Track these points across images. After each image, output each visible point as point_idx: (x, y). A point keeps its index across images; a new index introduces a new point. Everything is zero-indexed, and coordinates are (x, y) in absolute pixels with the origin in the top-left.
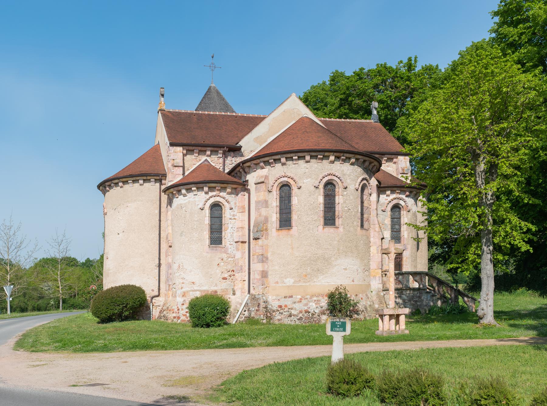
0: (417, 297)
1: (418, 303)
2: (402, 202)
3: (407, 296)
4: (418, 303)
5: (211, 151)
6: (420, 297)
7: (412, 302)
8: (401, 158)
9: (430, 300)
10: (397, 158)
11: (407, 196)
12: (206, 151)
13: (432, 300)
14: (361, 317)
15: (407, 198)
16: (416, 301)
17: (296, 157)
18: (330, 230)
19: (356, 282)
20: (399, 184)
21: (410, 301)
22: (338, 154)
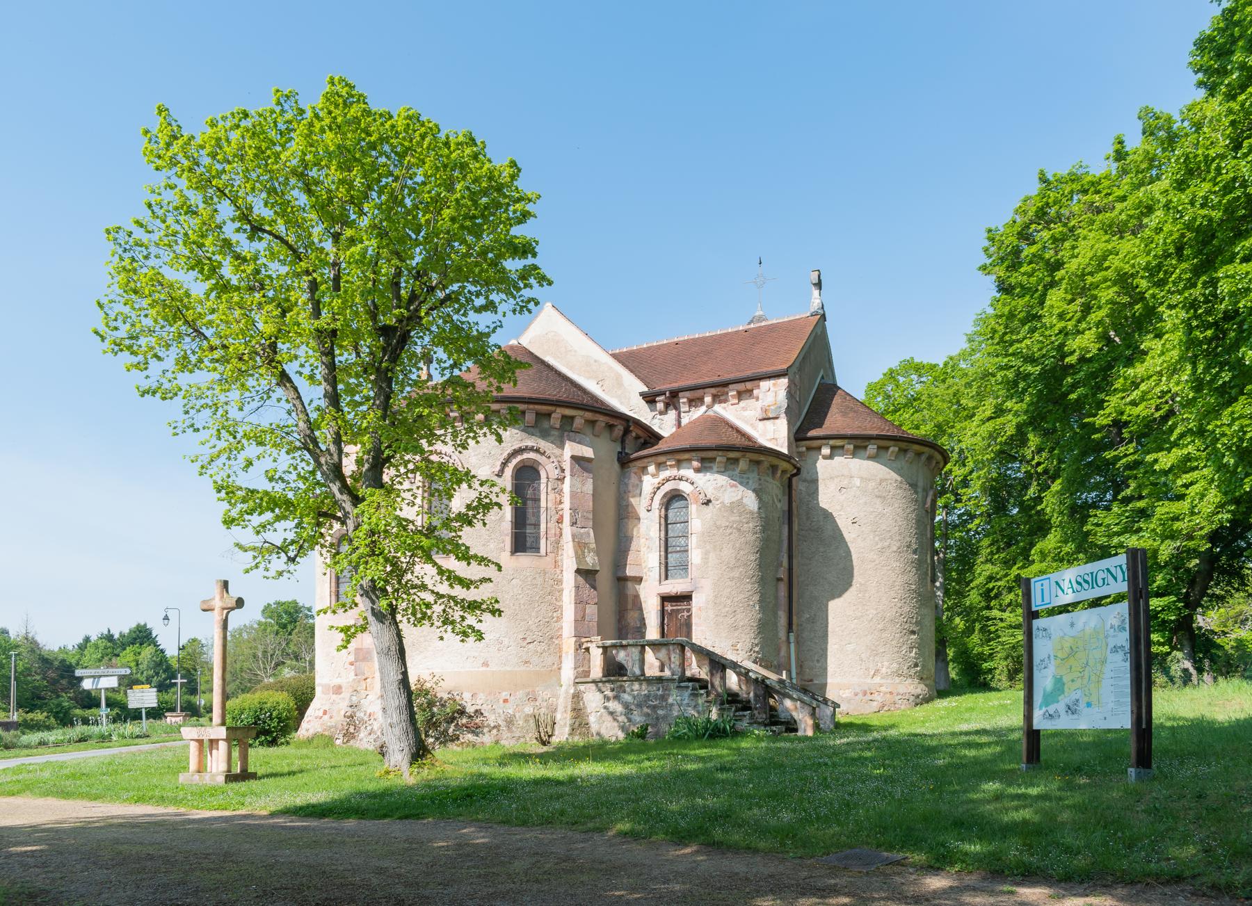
0: (656, 697)
1: (660, 712)
2: (685, 487)
3: (634, 697)
4: (660, 712)
5: (832, 448)
6: (663, 698)
7: (645, 710)
8: (764, 384)
9: (688, 705)
10: (758, 387)
11: (698, 470)
12: (819, 448)
13: (693, 703)
14: (487, 739)
15: (700, 475)
16: (654, 708)
17: (851, 447)
18: (524, 560)
19: (493, 667)
20: (577, 398)
21: (639, 706)
22: (904, 445)
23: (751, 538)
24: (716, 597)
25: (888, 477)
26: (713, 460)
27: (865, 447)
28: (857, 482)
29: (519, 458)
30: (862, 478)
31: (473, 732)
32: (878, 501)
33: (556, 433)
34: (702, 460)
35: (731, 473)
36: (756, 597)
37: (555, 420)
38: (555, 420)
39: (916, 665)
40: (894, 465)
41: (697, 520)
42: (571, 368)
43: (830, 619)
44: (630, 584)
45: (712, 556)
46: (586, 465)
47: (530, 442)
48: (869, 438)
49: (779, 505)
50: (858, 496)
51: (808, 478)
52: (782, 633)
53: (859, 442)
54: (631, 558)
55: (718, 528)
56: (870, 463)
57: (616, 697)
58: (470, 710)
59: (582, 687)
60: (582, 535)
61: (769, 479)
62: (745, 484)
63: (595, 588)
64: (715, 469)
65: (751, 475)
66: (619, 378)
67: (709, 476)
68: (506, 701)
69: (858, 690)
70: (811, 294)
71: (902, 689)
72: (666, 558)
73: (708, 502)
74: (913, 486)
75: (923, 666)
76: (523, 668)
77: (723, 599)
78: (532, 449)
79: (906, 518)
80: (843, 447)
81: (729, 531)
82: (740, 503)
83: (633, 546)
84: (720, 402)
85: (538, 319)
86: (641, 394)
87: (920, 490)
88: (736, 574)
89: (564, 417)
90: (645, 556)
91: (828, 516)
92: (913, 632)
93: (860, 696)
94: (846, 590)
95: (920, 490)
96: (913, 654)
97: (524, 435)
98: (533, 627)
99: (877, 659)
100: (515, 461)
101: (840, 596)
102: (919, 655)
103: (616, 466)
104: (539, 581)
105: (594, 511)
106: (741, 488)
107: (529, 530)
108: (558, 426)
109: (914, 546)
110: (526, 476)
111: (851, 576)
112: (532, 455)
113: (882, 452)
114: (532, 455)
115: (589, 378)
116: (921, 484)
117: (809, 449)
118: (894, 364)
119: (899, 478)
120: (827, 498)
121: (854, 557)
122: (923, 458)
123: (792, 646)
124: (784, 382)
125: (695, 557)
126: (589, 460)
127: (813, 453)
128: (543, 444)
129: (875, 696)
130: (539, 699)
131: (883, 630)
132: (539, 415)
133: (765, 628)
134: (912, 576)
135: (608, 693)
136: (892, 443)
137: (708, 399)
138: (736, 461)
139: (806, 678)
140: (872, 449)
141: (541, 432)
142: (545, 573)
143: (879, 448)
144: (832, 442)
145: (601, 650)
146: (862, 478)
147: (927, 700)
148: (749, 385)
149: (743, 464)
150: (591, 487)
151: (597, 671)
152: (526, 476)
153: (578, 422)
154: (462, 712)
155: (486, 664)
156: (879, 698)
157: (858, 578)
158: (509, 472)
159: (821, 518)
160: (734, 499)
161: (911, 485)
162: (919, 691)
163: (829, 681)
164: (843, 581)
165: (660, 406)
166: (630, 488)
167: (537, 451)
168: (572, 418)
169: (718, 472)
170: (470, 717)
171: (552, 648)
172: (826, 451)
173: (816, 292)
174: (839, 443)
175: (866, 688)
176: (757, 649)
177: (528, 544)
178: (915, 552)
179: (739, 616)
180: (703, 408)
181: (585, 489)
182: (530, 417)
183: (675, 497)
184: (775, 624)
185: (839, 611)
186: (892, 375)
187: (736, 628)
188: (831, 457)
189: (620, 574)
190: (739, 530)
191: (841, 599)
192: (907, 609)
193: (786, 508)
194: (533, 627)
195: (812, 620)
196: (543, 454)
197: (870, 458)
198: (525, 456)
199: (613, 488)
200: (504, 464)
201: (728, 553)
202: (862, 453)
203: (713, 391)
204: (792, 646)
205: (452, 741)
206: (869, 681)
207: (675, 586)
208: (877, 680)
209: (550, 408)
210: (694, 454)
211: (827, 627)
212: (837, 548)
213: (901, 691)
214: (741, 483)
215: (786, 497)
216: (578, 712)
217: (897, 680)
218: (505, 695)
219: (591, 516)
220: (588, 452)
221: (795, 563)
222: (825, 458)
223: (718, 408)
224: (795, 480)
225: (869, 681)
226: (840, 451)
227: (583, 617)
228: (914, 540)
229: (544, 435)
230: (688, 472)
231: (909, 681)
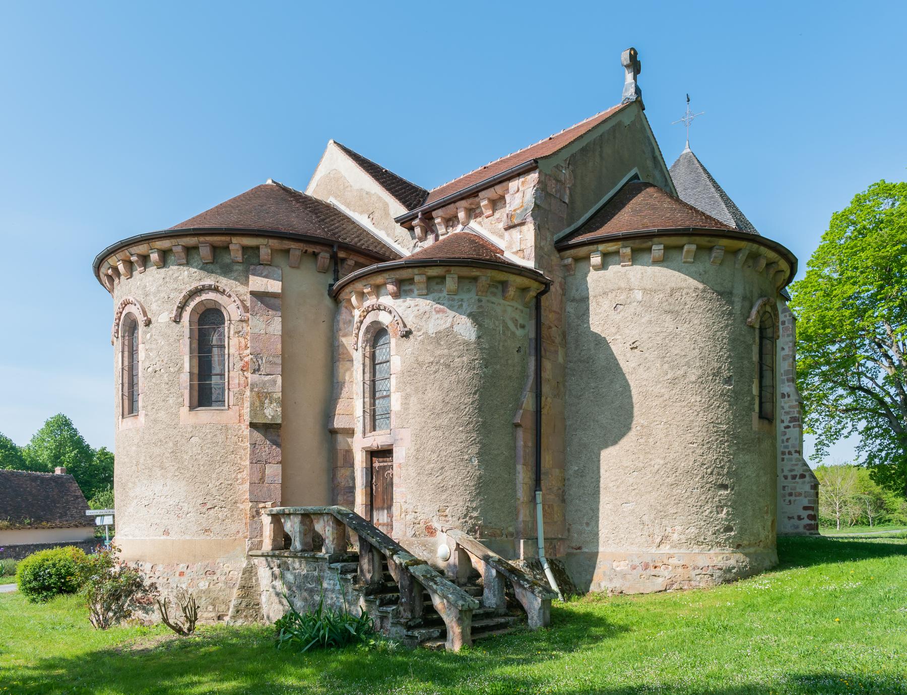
2: (385, 318)
8: (513, 185)
11: (396, 296)
12: (587, 258)
15: (399, 301)
17: (628, 251)
18: (205, 415)
19: (174, 536)
22: (704, 241)
23: (464, 375)
24: (418, 450)
25: (684, 285)
26: (411, 281)
27: (649, 250)
28: (639, 295)
29: (198, 300)
30: (644, 290)
31: (144, 608)
32: (668, 318)
33: (240, 268)
34: (399, 283)
35: (436, 295)
36: (475, 449)
37: (236, 253)
38: (236, 253)
39: (728, 529)
40: (693, 269)
41: (397, 356)
42: (348, 205)
43: (602, 471)
44: (340, 438)
45: (413, 400)
46: (272, 301)
47: (209, 281)
48: (649, 236)
49: (519, 332)
50: (643, 316)
51: (577, 297)
52: (522, 494)
53: (637, 244)
54: (340, 408)
55: (420, 364)
56: (657, 269)
57: (282, 577)
58: (147, 583)
59: (256, 561)
60: (264, 383)
61: (498, 300)
62: (458, 309)
63: (278, 445)
64: (416, 292)
65: (465, 296)
66: (386, 205)
67: (409, 301)
68: (181, 574)
69: (637, 562)
70: (624, 79)
71: (702, 561)
72: (374, 405)
73: (407, 334)
74: (725, 295)
75: (742, 531)
76: (202, 537)
77: (427, 454)
78: (210, 289)
79: (713, 337)
80: (617, 253)
81: (433, 368)
82: (449, 332)
83: (344, 394)
84: (476, 217)
85: (324, 159)
86: (397, 220)
87: (737, 300)
88: (444, 421)
89: (245, 249)
90: (352, 408)
91: (600, 342)
92: (724, 487)
93: (640, 570)
94: (623, 435)
95: (737, 300)
96: (723, 515)
97: (203, 274)
98: (214, 491)
99: (665, 522)
100: (192, 304)
101: (615, 443)
102: (732, 516)
103: (328, 302)
104: (220, 438)
105: (283, 355)
106: (452, 313)
107: (215, 380)
108: (240, 259)
109: (726, 374)
110: (207, 323)
111: (630, 416)
112: (211, 296)
113: (674, 254)
114: (211, 296)
115: (361, 213)
116: (739, 290)
117: (577, 260)
118: (863, 188)
119: (693, 283)
120: (601, 319)
121: (634, 392)
122: (741, 256)
123: (540, 508)
124: (534, 177)
125: (396, 402)
126: (274, 295)
127: (582, 265)
128: (224, 282)
129: (661, 571)
130: (218, 572)
131: (675, 484)
132: (214, 248)
133: (490, 489)
134: (722, 413)
135: (277, 570)
136: (684, 240)
137: (461, 215)
138: (442, 279)
139: (574, 545)
140: (657, 250)
141: (221, 268)
142: (227, 429)
143: (667, 248)
144: (601, 247)
145: (270, 518)
146: (644, 290)
147: (746, 574)
148: (499, 189)
149: (451, 283)
150: (279, 327)
151: (267, 546)
152: (207, 323)
153: (265, 253)
154: (139, 585)
155: (166, 532)
156: (666, 573)
157: (639, 419)
158: (186, 316)
159: (592, 345)
160: (441, 328)
161: (720, 294)
162: (732, 562)
163: (601, 549)
164: (620, 423)
165: (418, 231)
166: (341, 325)
167: (216, 289)
168: (257, 248)
169: (420, 296)
170: (145, 591)
171: (236, 514)
172: (596, 260)
173: (629, 77)
174: (611, 247)
175: (648, 559)
176: (475, 514)
177: (213, 399)
178: (728, 381)
179: (449, 473)
180: (460, 227)
181: (270, 329)
182: (205, 252)
183: (377, 333)
184: (513, 482)
185: (613, 462)
186: (859, 201)
187: (444, 489)
188: (603, 266)
189: (330, 427)
190: (448, 366)
191: (617, 447)
192: (711, 456)
193: (532, 335)
194: (214, 491)
195: (581, 474)
196: (223, 293)
197: (656, 262)
198: (204, 297)
199: (323, 327)
200: (182, 308)
201: (433, 395)
202: (646, 257)
203: (464, 203)
204: (540, 508)
205: (125, 617)
206: (653, 550)
207: (378, 440)
208: (666, 549)
209: (223, 238)
210: (386, 275)
211: (598, 481)
212: (612, 382)
213: (701, 565)
214: (451, 307)
215: (533, 322)
216: (248, 589)
217: (696, 549)
218: (182, 567)
219: (279, 361)
220: (274, 286)
221: (540, 406)
222: (597, 268)
223: (473, 224)
224: (543, 298)
225: (653, 550)
226: (617, 258)
227: (262, 480)
228: (725, 366)
229: (226, 271)
230: (386, 300)
231: (717, 550)
